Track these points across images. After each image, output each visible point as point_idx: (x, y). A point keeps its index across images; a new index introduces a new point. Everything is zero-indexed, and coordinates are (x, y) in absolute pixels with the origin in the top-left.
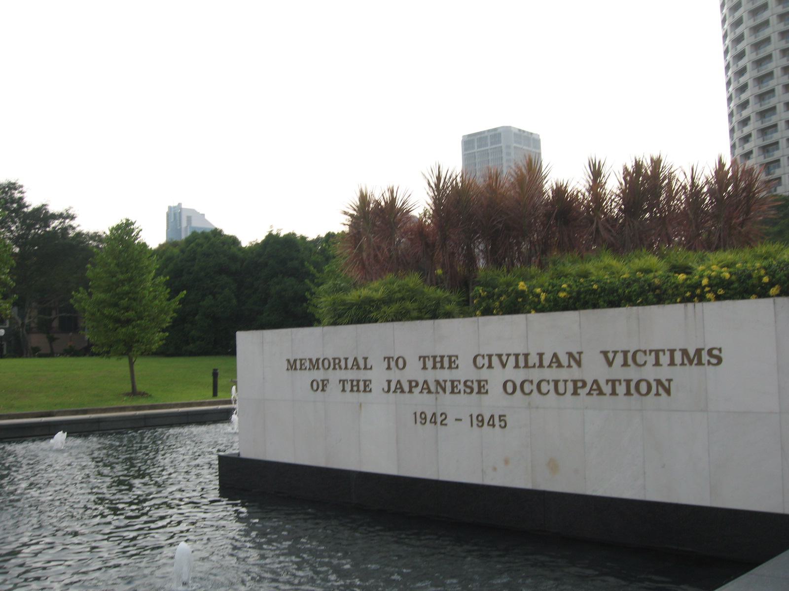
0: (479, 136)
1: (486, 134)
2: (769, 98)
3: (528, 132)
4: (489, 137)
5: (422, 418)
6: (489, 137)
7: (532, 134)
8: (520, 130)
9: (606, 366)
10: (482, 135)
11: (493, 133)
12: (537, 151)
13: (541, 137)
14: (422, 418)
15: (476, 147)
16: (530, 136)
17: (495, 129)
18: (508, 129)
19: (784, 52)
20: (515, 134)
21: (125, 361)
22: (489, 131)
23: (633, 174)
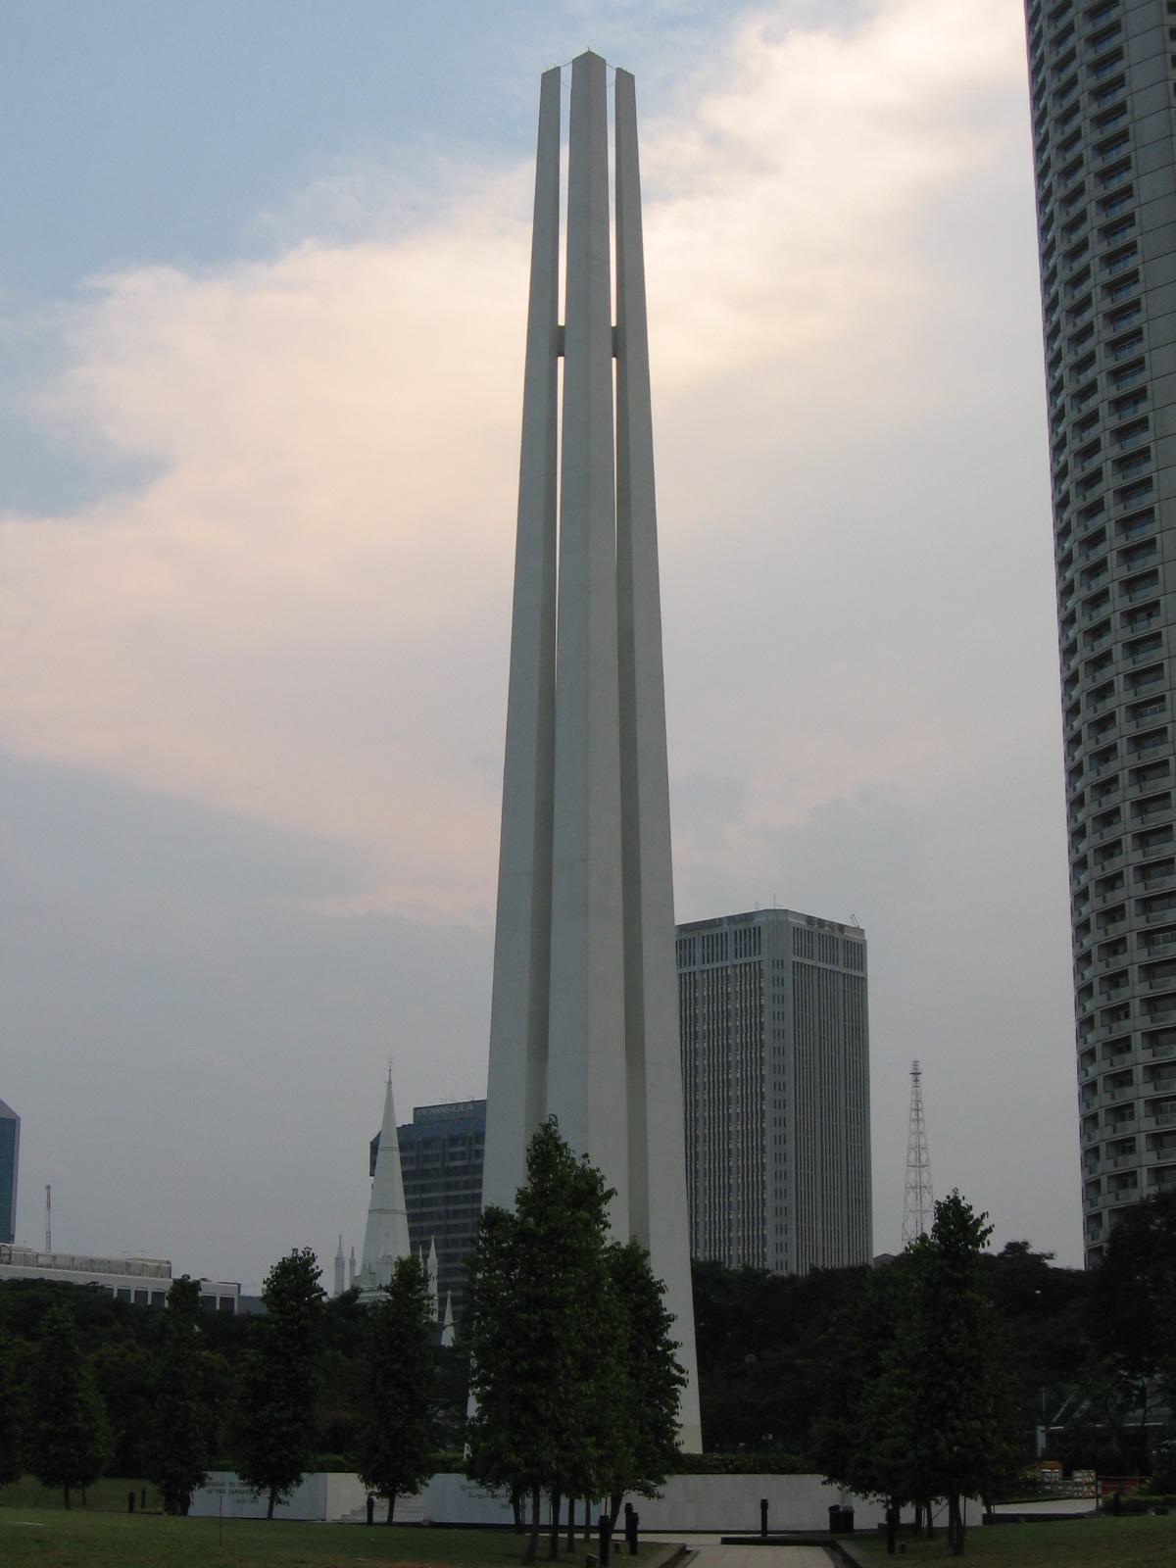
0: (706, 933)
1: (725, 927)
2: (1133, 375)
3: (831, 924)
4: (731, 938)
5: (239, 1501)
6: (731, 938)
7: (842, 928)
8: (810, 920)
9: (771, 1504)
10: (717, 931)
11: (741, 927)
12: (860, 974)
13: (867, 936)
14: (239, 1501)
15: (731, 954)
16: (837, 934)
17: (747, 917)
18: (778, 917)
19: (1158, 1173)
20: (797, 930)
21: (55, 1251)
22: (731, 919)
23: (606, 1251)
